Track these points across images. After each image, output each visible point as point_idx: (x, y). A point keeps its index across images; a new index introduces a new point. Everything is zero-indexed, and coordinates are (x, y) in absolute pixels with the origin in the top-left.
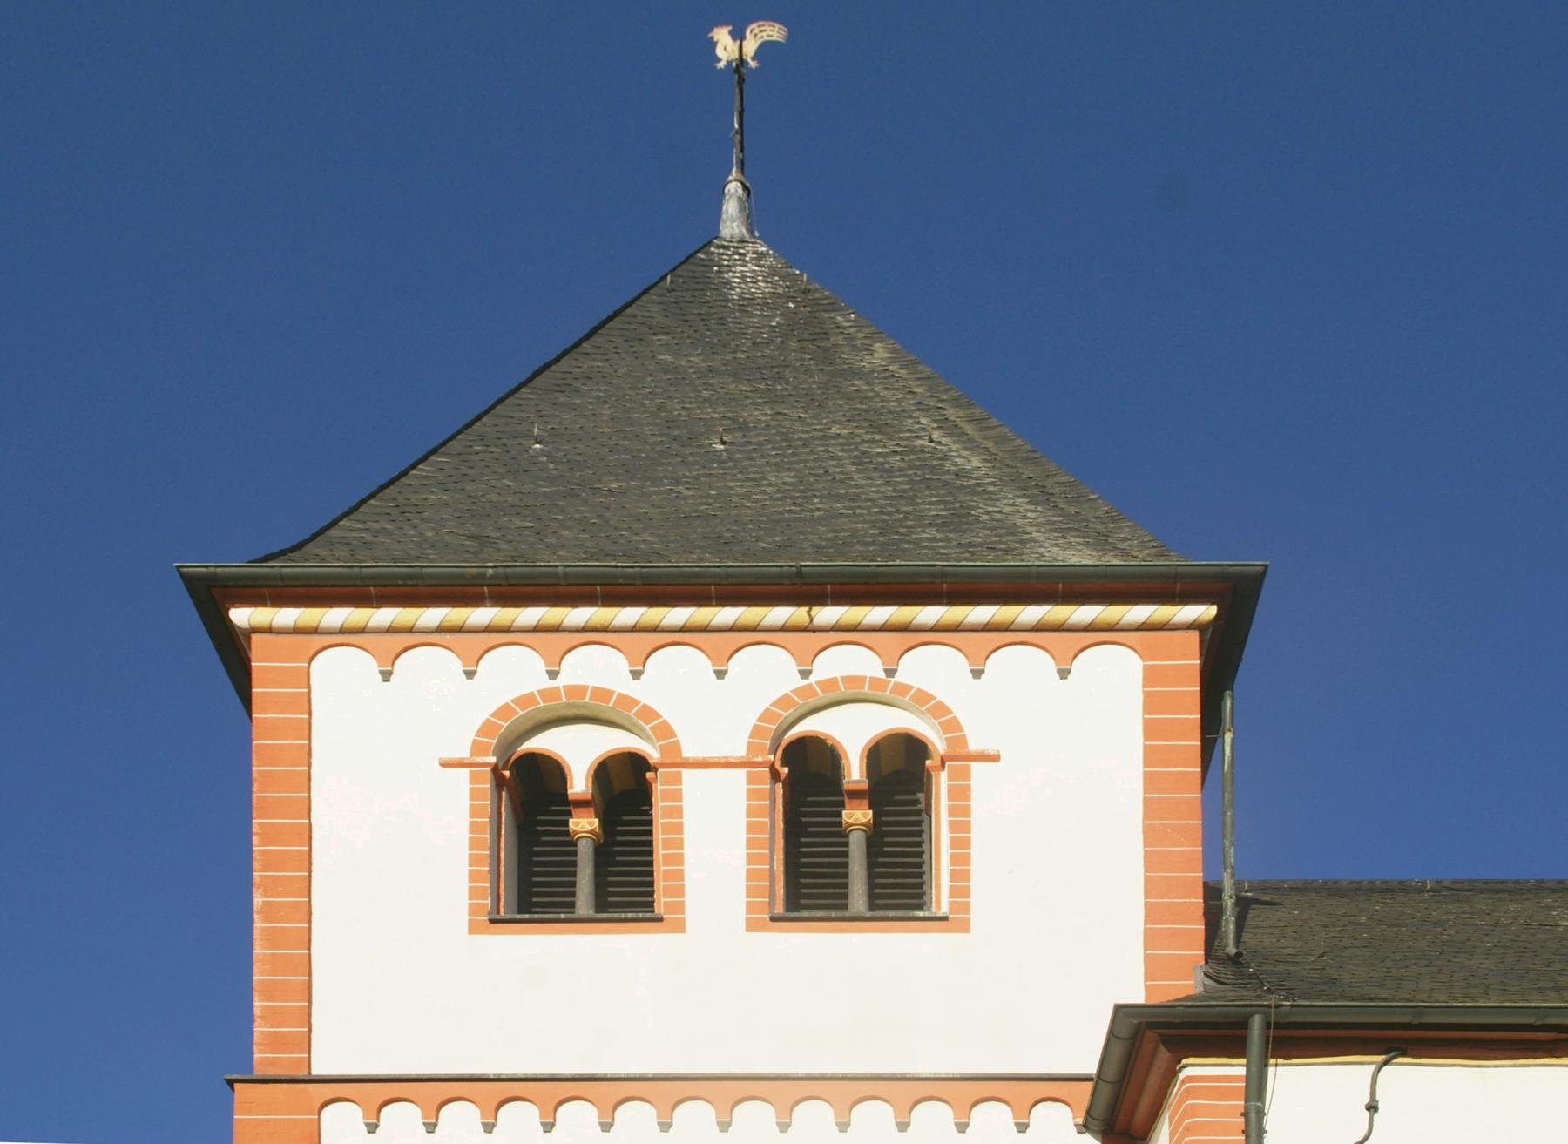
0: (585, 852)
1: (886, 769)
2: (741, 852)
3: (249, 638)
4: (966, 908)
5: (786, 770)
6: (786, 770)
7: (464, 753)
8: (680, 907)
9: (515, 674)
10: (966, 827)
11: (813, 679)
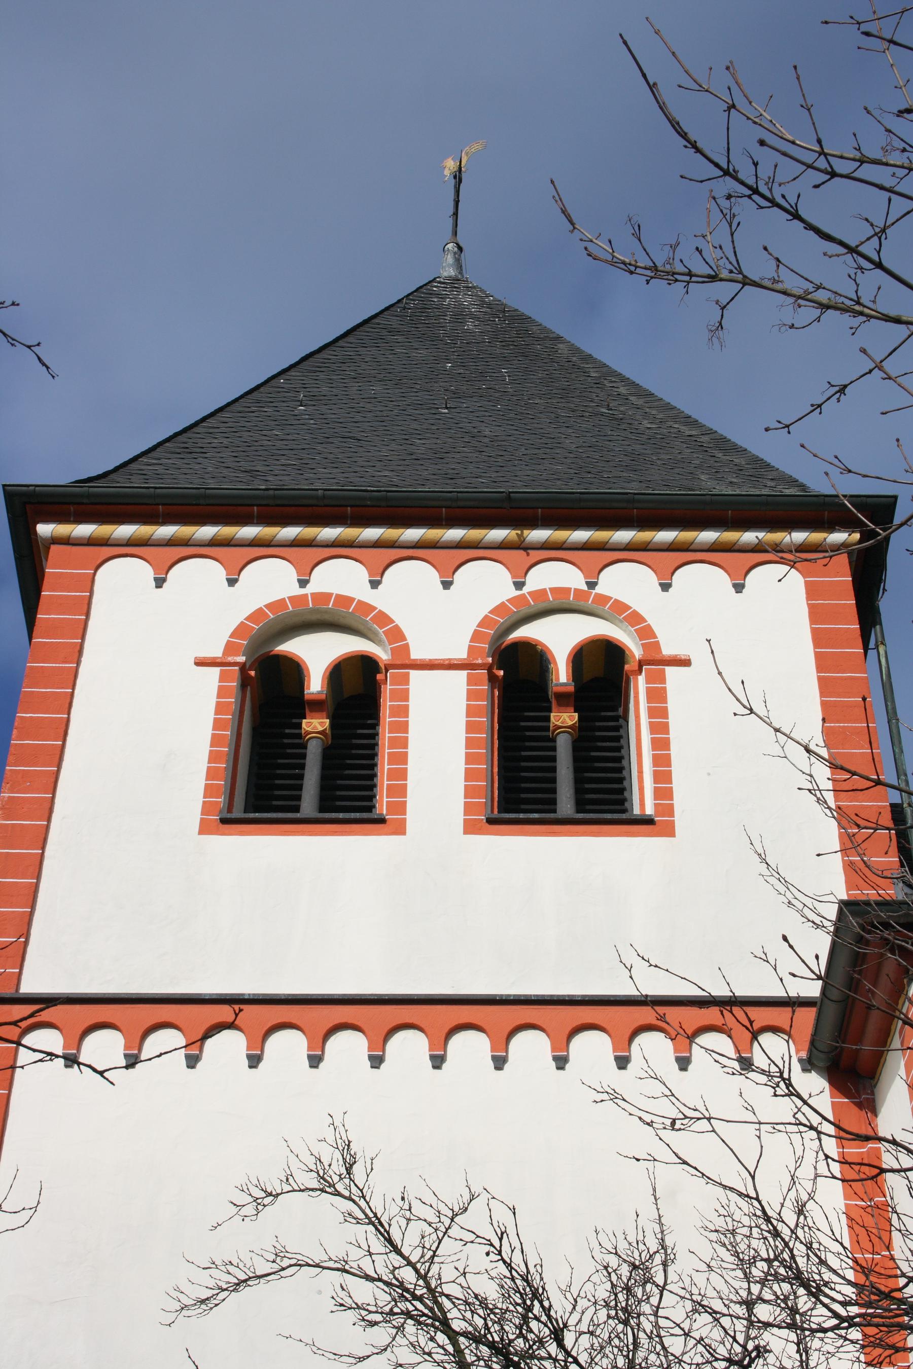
0: (314, 753)
1: (587, 677)
2: (460, 751)
3: (48, 549)
4: (669, 810)
5: (502, 673)
6: (502, 673)
7: (217, 652)
8: (401, 808)
9: (272, 581)
10: (665, 728)
11: (526, 590)
